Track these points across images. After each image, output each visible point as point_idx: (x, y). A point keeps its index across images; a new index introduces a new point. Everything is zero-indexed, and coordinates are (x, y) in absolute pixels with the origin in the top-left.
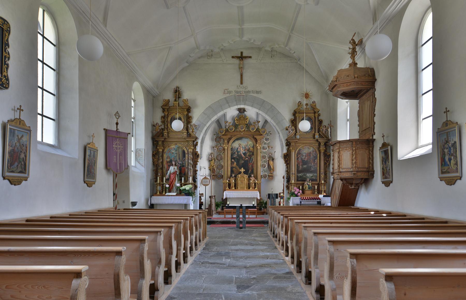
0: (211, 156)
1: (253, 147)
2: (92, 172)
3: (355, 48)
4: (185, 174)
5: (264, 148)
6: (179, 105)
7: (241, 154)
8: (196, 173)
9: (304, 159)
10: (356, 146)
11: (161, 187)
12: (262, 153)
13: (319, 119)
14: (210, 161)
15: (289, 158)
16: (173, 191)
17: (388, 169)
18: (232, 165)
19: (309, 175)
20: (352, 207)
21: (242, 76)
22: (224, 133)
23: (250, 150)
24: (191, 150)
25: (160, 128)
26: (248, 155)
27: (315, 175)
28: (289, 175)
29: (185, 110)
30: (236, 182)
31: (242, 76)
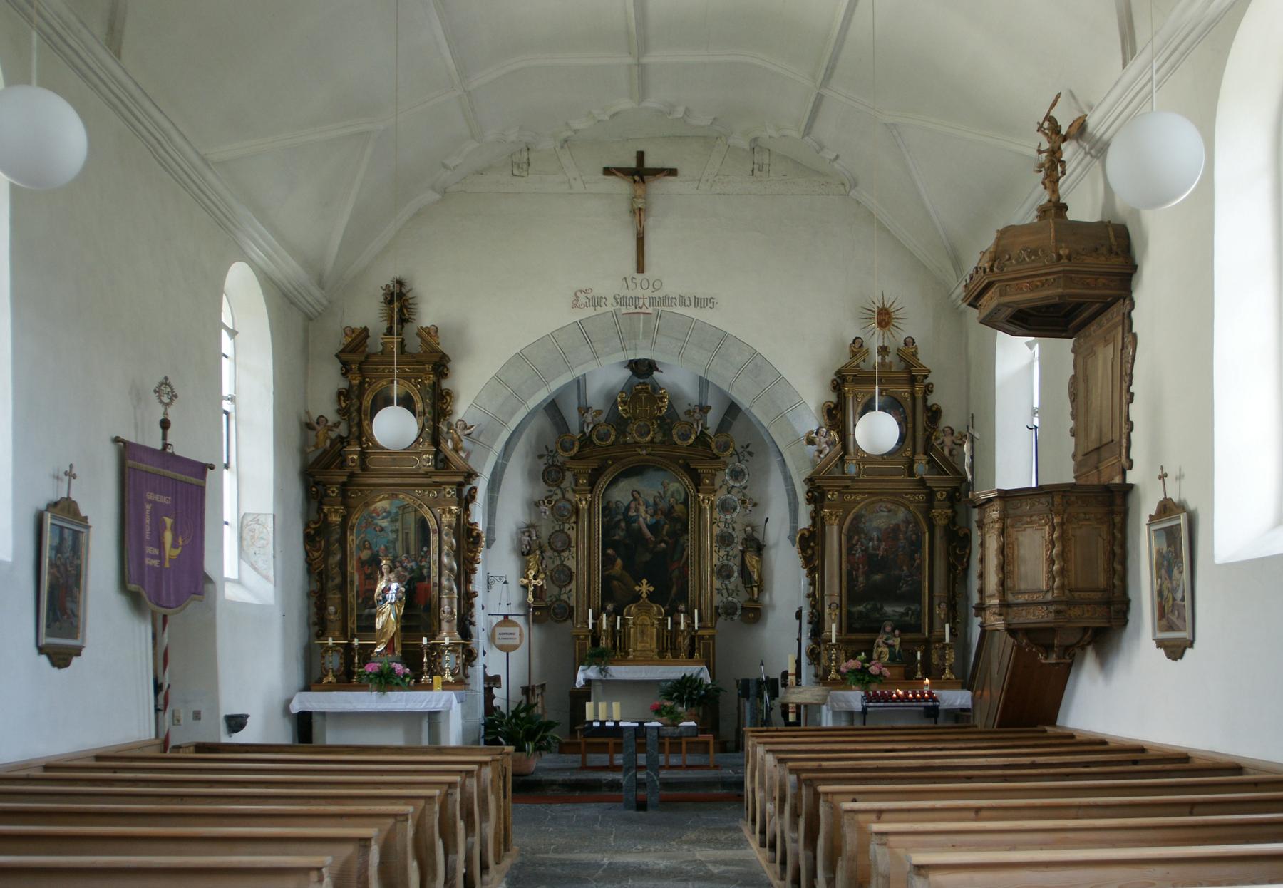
0: (530, 536)
2: (69, 612)
3: (1059, 148)
5: (726, 507)
6: (406, 348)
7: (640, 529)
8: (472, 605)
9: (873, 552)
10: (1064, 511)
11: (339, 657)
14: (524, 553)
17: (1179, 596)
19: (894, 611)
20: (1047, 728)
22: (576, 449)
23: (675, 515)
25: (333, 435)
26: (667, 532)
27: (913, 608)
28: (817, 611)
29: (429, 367)
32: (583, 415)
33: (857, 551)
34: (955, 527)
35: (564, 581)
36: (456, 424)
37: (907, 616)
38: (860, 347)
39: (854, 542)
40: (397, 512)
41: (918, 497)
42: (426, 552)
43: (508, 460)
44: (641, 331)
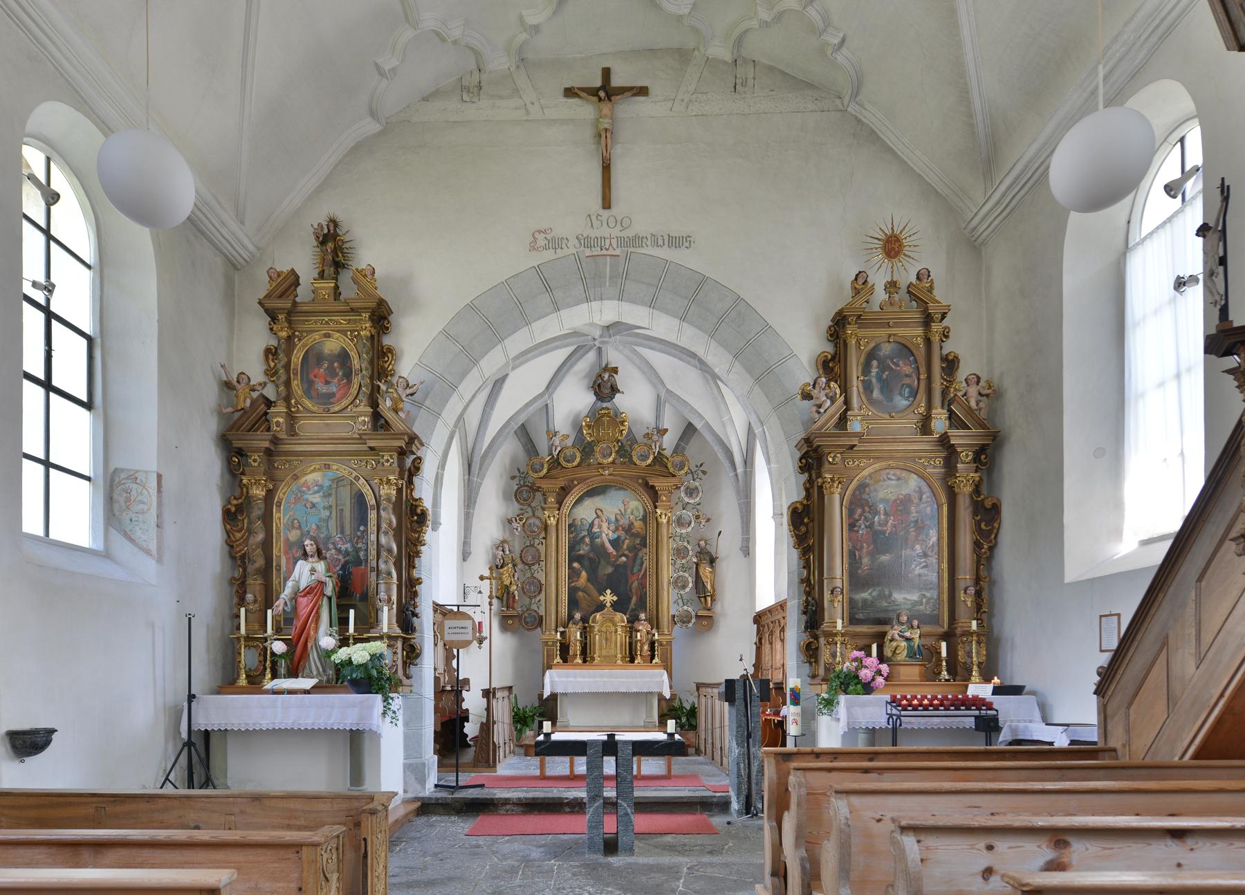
0: (503, 551)
1: (644, 519)
4: (365, 597)
5: (680, 522)
7: (603, 545)
8: (415, 594)
12: (674, 540)
13: (945, 352)
15: (816, 523)
16: (307, 671)
18: (573, 582)
19: (905, 599)
21: (606, 168)
22: (545, 471)
24: (388, 491)
26: (627, 546)
27: (928, 595)
29: (366, 315)
30: (586, 638)
31: (606, 168)
32: (552, 438)
33: (860, 526)
34: (979, 497)
35: (535, 592)
36: (397, 383)
37: (922, 605)
38: (863, 284)
39: (857, 517)
40: (330, 486)
41: (934, 461)
42: (364, 531)
43: (483, 479)
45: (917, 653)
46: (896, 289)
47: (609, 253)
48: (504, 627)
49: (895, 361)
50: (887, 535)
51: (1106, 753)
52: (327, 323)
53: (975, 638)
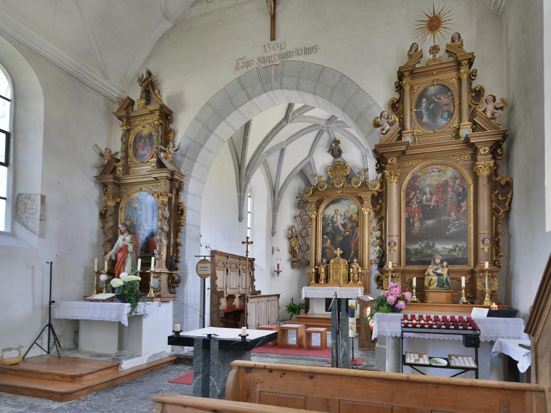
1: (358, 213)
7: (338, 227)
8: (178, 251)
9: (427, 203)
13: (473, 86)
18: (324, 245)
19: (444, 248)
21: (273, 18)
22: (311, 193)
26: (349, 227)
31: (273, 18)
33: (413, 203)
34: (497, 178)
38: (415, 51)
39: (411, 197)
41: (464, 157)
43: (281, 199)
44: (273, 76)
45: (445, 284)
46: (436, 51)
47: (274, 63)
48: (293, 266)
49: (438, 96)
50: (431, 207)
51: (534, 393)
52: (144, 120)
53: (487, 274)
